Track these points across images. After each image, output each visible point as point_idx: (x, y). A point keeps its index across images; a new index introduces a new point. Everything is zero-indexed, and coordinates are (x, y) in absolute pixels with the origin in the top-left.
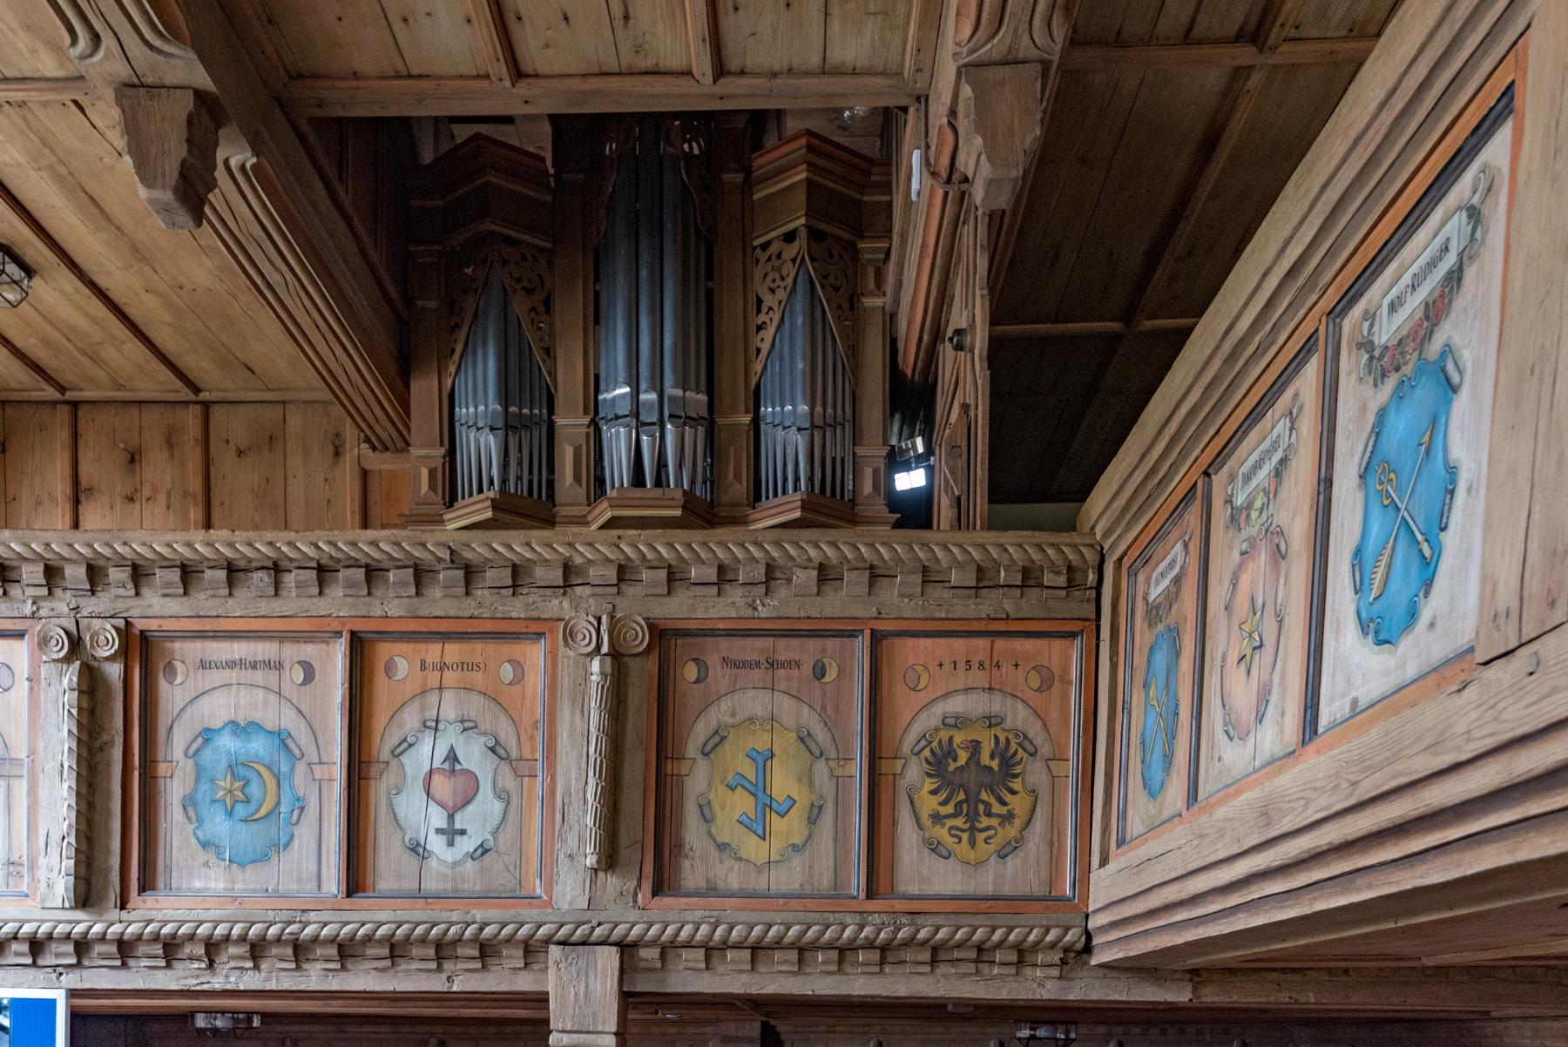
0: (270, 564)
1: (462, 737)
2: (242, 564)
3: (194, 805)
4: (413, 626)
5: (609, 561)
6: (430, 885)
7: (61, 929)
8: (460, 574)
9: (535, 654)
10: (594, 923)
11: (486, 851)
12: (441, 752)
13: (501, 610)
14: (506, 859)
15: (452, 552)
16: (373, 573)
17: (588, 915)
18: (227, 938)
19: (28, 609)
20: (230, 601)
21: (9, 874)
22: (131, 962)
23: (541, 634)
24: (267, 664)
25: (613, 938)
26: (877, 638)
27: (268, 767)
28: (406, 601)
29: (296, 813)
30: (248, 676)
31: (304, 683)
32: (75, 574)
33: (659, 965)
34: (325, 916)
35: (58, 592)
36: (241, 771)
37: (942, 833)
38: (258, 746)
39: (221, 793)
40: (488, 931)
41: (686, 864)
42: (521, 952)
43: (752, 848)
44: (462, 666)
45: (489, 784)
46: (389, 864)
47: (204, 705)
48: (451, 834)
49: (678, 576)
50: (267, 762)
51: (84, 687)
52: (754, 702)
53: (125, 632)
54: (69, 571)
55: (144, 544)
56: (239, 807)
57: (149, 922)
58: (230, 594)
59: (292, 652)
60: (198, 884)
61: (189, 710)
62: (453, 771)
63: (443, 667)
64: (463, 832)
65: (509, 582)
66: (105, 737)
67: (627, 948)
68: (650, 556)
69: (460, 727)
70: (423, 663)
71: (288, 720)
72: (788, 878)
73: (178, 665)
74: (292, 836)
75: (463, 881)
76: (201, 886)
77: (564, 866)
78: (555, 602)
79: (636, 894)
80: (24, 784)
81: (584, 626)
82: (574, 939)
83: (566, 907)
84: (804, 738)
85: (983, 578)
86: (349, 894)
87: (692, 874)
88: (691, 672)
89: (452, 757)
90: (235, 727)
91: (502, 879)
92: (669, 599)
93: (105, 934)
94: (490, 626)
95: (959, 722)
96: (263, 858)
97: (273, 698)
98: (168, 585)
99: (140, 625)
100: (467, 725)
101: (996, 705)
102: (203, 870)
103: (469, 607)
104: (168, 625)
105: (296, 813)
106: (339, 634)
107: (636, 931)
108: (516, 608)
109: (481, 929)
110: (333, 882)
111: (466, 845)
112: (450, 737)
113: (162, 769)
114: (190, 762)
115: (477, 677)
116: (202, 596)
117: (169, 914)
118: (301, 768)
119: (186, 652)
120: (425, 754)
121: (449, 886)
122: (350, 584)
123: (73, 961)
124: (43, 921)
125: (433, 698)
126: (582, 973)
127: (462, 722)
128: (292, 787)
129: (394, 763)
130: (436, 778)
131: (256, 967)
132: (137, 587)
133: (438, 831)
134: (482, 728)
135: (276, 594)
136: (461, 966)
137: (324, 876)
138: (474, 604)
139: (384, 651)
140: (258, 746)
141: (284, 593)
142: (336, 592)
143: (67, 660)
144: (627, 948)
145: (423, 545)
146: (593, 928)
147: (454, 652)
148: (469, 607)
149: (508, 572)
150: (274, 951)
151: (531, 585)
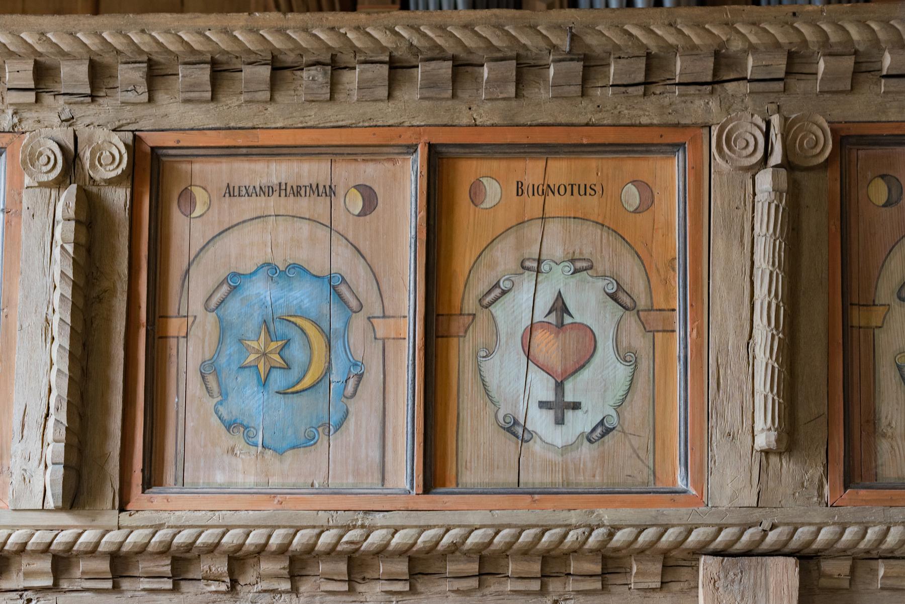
0: (327, 58)
1: (572, 281)
2: (290, 58)
3: (217, 373)
4: (510, 136)
5: (778, 45)
6: (533, 477)
7: (39, 538)
8: (578, 66)
9: (671, 172)
10: (766, 525)
11: (608, 431)
12: (545, 301)
13: (628, 115)
14: (635, 442)
15: (574, 37)
16: (462, 68)
17: (757, 514)
18: (261, 551)
20: (271, 109)
22: (126, 584)
23: (679, 146)
24: (315, 190)
25: (794, 544)
27: (315, 323)
28: (501, 104)
29: (352, 383)
30: (290, 204)
31: (363, 213)
32: (74, 74)
33: (846, 584)
34: (396, 519)
35: (48, 99)
36: (279, 328)
38: (303, 296)
39: (252, 357)
40: (620, 537)
41: (884, 445)
42: (659, 567)
44: (572, 189)
45: (610, 343)
46: (477, 449)
47: (231, 244)
48: (561, 408)
49: (864, 67)
50: (313, 315)
51: (83, 218)
53: (135, 147)
54: (65, 69)
55: (167, 32)
56: (276, 375)
57: (157, 528)
58: (272, 99)
59: (347, 173)
60: (220, 478)
61: (211, 249)
62: (561, 325)
63: (547, 190)
64: (576, 406)
65: (641, 78)
66: (106, 284)
67: (807, 559)
68: (834, 37)
69: (569, 268)
70: (520, 185)
71: (343, 261)
73: (198, 192)
74: (347, 412)
75: (577, 470)
76: (224, 478)
77: (720, 449)
78: (699, 103)
79: (821, 487)
81: (749, 130)
82: (738, 546)
83: (724, 504)
86: (427, 490)
88: (879, 192)
89: (560, 307)
90: (271, 270)
91: (628, 466)
92: (851, 98)
93: (98, 544)
94: (612, 136)
96: (310, 441)
97: (322, 233)
98: (192, 87)
99: (152, 140)
100: (579, 265)
102: (227, 458)
103: (585, 111)
104: (188, 140)
105: (352, 383)
106: (411, 149)
107: (825, 535)
108: (648, 111)
109: (611, 535)
110: (403, 470)
111: (580, 423)
112: (559, 279)
113: (175, 326)
114: (212, 317)
115: (591, 203)
116: (234, 101)
117: (185, 517)
118: (359, 321)
119: (208, 174)
120: (522, 305)
121: (559, 478)
123: (49, 582)
124: (14, 528)
125: (534, 230)
126: (749, 594)
127: (573, 261)
128: (346, 348)
129: (482, 315)
130: (540, 337)
131: (295, 590)
132: (151, 90)
133: (543, 405)
134: (600, 268)
135: (332, 98)
136: (571, 586)
137: (389, 466)
138: (591, 107)
139: (468, 170)
140: (303, 296)
141: (341, 96)
142: (410, 94)
143: (60, 183)
144: (807, 559)
145: (534, 27)
146: (765, 533)
147: (560, 170)
148: (585, 111)
149: (642, 64)
150: (322, 567)
151: (670, 82)
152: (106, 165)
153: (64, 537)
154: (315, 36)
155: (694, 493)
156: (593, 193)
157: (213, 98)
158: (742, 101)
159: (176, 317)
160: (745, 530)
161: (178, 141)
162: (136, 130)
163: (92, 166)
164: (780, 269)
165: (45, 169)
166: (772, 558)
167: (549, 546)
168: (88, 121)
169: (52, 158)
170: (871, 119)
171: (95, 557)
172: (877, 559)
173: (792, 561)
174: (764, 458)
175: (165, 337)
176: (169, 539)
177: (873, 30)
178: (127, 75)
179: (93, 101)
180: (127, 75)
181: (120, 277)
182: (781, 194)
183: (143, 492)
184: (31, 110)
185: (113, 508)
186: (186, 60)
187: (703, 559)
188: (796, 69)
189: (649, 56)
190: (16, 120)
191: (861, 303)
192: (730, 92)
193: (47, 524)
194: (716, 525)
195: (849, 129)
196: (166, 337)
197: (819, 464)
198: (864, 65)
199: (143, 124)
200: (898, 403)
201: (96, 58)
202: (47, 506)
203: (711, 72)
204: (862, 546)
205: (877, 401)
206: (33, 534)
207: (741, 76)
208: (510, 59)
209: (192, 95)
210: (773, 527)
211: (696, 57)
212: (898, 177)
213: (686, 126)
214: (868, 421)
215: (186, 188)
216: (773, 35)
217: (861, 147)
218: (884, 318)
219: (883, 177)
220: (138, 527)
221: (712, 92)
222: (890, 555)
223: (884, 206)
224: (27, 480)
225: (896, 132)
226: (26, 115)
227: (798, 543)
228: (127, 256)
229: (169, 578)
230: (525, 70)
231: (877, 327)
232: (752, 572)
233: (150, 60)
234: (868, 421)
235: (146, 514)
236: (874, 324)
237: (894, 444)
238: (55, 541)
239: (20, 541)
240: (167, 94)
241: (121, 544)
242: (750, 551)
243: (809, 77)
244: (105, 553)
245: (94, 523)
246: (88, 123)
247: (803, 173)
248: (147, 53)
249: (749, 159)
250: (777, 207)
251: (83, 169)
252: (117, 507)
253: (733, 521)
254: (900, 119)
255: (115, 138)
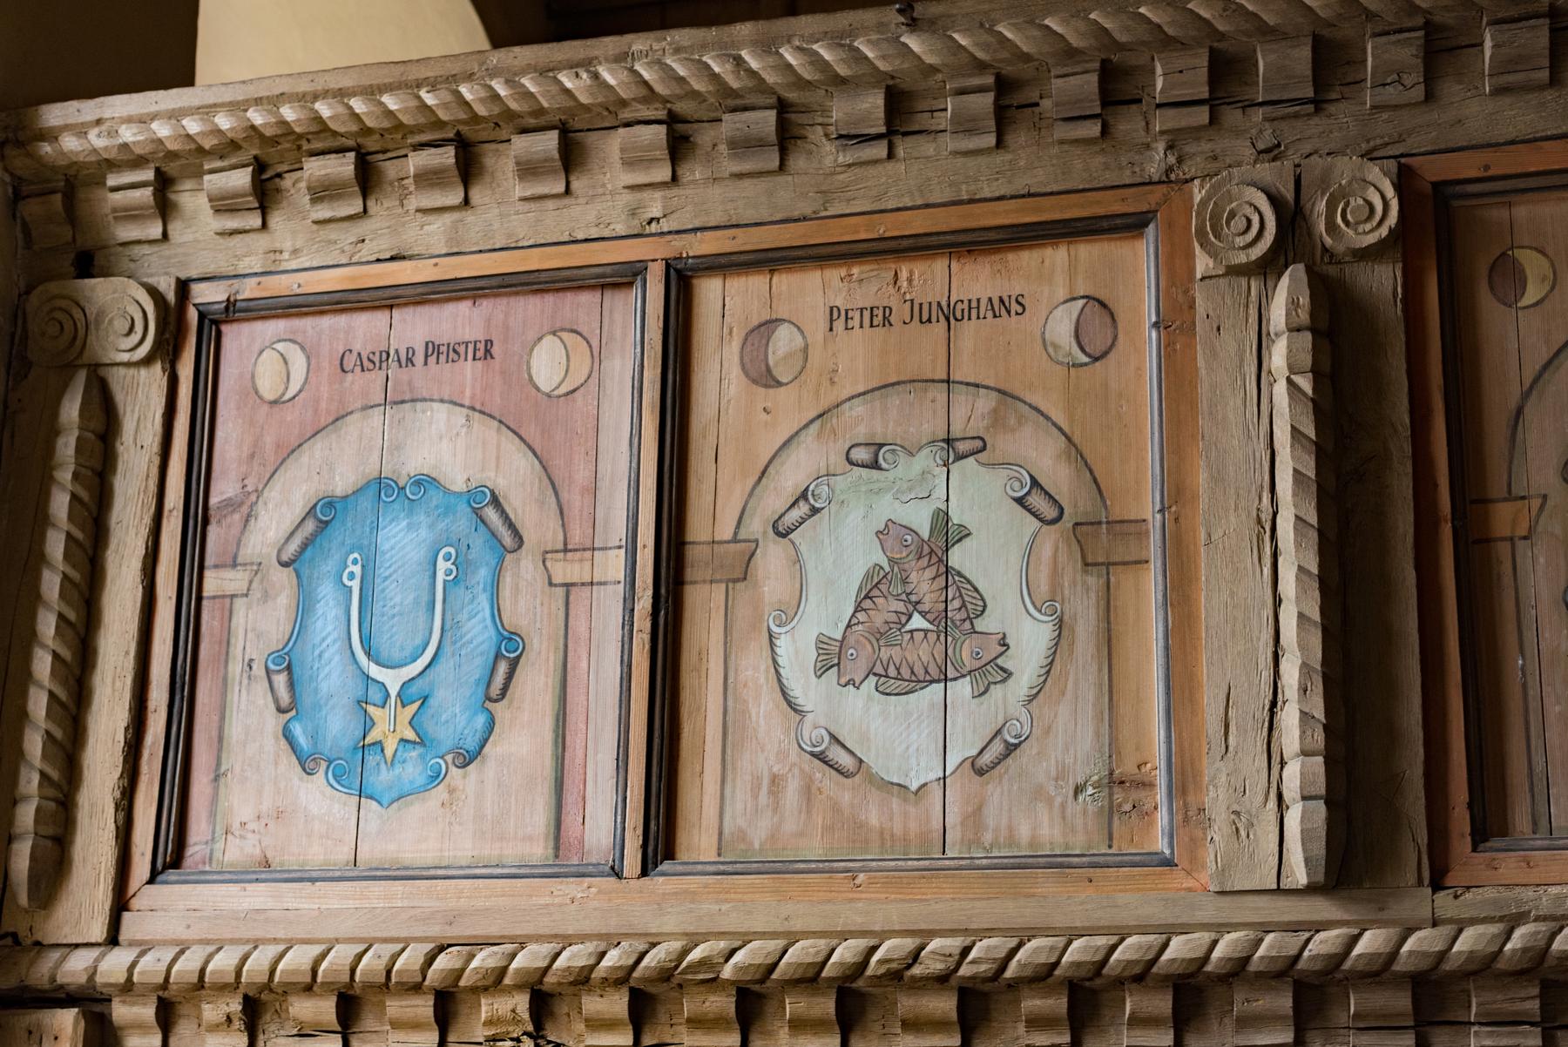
19: (1156, 161)
21: (1111, 810)
57: (1513, 922)
65: (1204, 92)
80: (1151, 582)
93: (1394, 955)
99: (1434, 170)
103: (786, 195)
104: (1503, 163)
113: (1503, 518)
122: (224, 205)
142: (823, 156)
152: (1358, 223)
153: (1324, 943)
156: (1020, 310)
159: (1505, 500)
161: (1487, 168)
162: (1402, 156)
163: (1331, 227)
165: (1240, 241)
168: (1308, 148)
169: (1256, 219)
171: (1380, 983)
175: (1487, 541)
176: (1542, 943)
178: (1386, 56)
179: (1318, 110)
180: (1386, 56)
181: (1396, 431)
183: (1474, 850)
184: (1198, 139)
185: (1420, 883)
186: (1500, 15)
190: (1172, 159)
193: (1286, 918)
196: (1488, 541)
199: (1413, 144)
201: (1325, 32)
202: (1286, 883)
206: (1262, 940)
208: (349, 150)
209: (1511, 78)
215: (1504, 254)
220: (1473, 921)
224: (1243, 833)
226: (1190, 148)
228: (1406, 389)
229: (1532, 1024)
233: (1428, 26)
235: (1489, 893)
238: (1306, 953)
239: (1237, 955)
240: (1460, 83)
241: (1442, 955)
244: (1404, 975)
245: (1384, 915)
246: (1308, 151)
248: (665, 101)
251: (1310, 234)
252: (1426, 882)
255: (1374, 172)
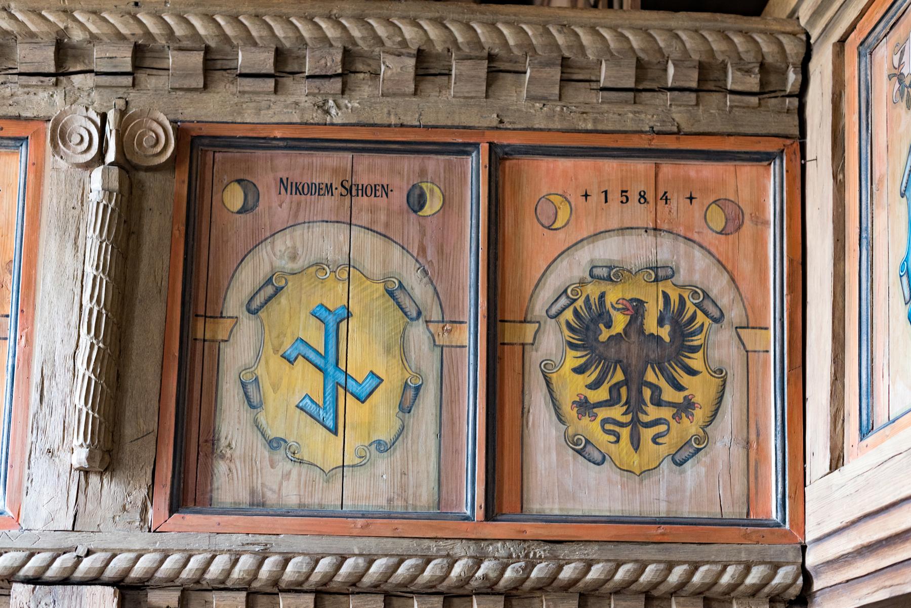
5: (121, 37)
10: (81, 551)
26: (499, 157)
37: (592, 428)
41: (221, 467)
43: (317, 444)
52: (323, 241)
72: (370, 489)
78: (43, 95)
79: (144, 510)
81: (82, 124)
82: (50, 573)
83: (39, 526)
84: (395, 292)
85: (645, 78)
87: (229, 482)
88: (234, 198)
92: (205, 96)
93: (103, 570)
95: (614, 274)
101: (665, 251)
145: (493, 25)
146: (79, 559)
154: (703, 36)
155: (11, 514)
157: (415, 93)
158: (89, 95)
160: (59, 555)
164: (104, 274)
166: (89, 587)
167: (700, 587)
170: (225, 120)
172: (211, 590)
173: (110, 590)
174: (82, 477)
177: (219, 25)
182: (111, 193)
187: (15, 585)
188: (147, 63)
189: (207, 50)
191: (208, 314)
192: (77, 85)
194: (27, 549)
195: (201, 129)
197: (144, 486)
198: (220, 62)
200: (239, 423)
203: (53, 63)
204: (184, 575)
205: (217, 420)
207: (88, 68)
210: (89, 553)
211: (35, 46)
212: (256, 183)
213: (27, 119)
214: (206, 441)
216: (113, 25)
217: (217, 149)
218: (231, 331)
219: (239, 181)
221: (56, 84)
222: (222, 586)
223: (239, 212)
225: (251, 134)
227: (115, 571)
230: (496, 69)
231: (223, 341)
232: (66, 602)
234: (206, 441)
236: (220, 338)
237: (233, 466)
241: (129, 570)
242: (39, 578)
243: (161, 72)
247: (149, 174)
249: (84, 155)
250: (106, 207)
253: (45, 546)
254: (256, 121)
